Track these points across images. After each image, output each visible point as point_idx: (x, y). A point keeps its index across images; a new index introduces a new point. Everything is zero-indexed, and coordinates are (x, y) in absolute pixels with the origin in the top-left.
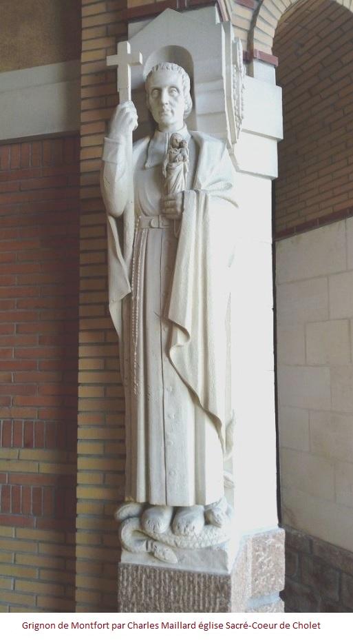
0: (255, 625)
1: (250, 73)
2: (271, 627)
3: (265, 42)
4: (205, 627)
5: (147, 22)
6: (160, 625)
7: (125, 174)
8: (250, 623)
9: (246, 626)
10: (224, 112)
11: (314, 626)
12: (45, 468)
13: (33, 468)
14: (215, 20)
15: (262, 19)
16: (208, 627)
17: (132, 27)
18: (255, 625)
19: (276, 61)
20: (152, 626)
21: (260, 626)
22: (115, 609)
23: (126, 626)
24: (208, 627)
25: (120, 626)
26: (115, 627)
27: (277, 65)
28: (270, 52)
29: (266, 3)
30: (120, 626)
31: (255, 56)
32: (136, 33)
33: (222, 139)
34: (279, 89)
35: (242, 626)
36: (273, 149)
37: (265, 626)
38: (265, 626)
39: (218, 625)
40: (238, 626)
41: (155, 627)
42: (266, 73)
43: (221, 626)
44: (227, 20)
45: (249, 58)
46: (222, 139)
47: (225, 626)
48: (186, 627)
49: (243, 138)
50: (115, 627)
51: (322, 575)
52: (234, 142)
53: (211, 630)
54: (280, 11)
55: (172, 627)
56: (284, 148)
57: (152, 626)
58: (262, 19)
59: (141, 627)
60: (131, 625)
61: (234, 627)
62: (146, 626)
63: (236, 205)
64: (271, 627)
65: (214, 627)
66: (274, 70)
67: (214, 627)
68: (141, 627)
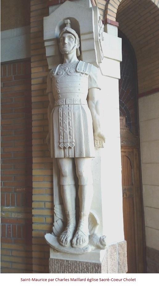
0: (113, 280)
1: (105, 30)
2: (120, 280)
3: (112, 17)
4: (90, 280)
5: (58, 6)
6: (70, 280)
7: (75, 243)
8: (110, 279)
9: (108, 280)
10: (94, 50)
11: (133, 280)
12: (20, 216)
13: (14, 215)
14: (89, 5)
15: (112, 5)
16: (91, 280)
17: (51, 9)
18: (113, 280)
19: (117, 24)
20: (66, 280)
21: (115, 280)
22: (48, 272)
23: (54, 280)
24: (91, 280)
25: (52, 280)
26: (49, 280)
27: (118, 26)
28: (114, 20)
29: (111, 2)
30: (52, 280)
31: (108, 22)
32: (53, 11)
33: (92, 91)
34: (120, 40)
35: (107, 280)
36: (118, 64)
37: (117, 280)
38: (117, 280)
39: (96, 280)
40: (105, 280)
41: (68, 280)
42: (113, 30)
43: (97, 280)
44: (95, 5)
45: (105, 22)
46: (92, 91)
47: (99, 280)
48: (81, 280)
49: (104, 61)
50: (49, 280)
51: (140, 260)
52: (100, 62)
53: (92, 282)
54: (117, 5)
55: (75, 280)
56: (123, 65)
57: (66, 280)
58: (112, 5)
59: (62, 280)
60: (125, 280)
61: (103, 280)
62: (64, 280)
63: (100, 89)
64: (120, 280)
65: (94, 280)
66: (117, 29)
67: (94, 280)
68: (62, 280)
